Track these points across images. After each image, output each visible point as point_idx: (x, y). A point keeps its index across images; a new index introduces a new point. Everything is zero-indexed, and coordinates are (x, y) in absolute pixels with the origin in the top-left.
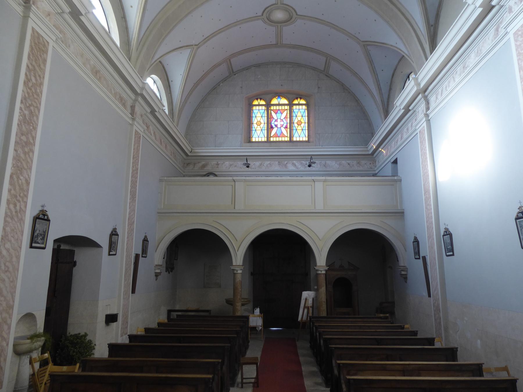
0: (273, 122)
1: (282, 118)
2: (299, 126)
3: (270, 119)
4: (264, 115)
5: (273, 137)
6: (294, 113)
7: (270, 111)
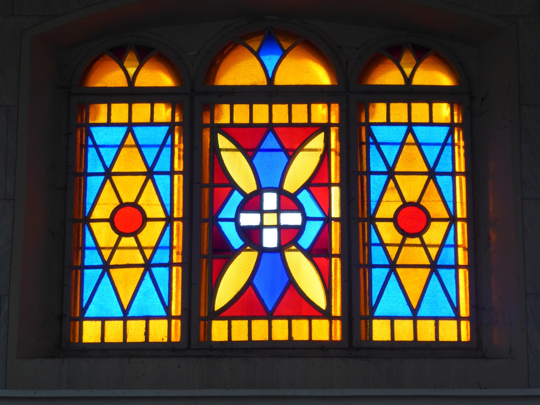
0: (229, 211)
1: (290, 186)
2: (409, 241)
3: (207, 191)
4: (163, 165)
5: (230, 319)
6: (373, 148)
7: (207, 135)
